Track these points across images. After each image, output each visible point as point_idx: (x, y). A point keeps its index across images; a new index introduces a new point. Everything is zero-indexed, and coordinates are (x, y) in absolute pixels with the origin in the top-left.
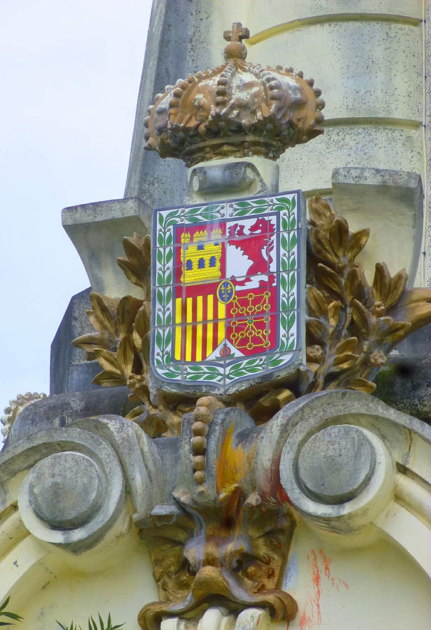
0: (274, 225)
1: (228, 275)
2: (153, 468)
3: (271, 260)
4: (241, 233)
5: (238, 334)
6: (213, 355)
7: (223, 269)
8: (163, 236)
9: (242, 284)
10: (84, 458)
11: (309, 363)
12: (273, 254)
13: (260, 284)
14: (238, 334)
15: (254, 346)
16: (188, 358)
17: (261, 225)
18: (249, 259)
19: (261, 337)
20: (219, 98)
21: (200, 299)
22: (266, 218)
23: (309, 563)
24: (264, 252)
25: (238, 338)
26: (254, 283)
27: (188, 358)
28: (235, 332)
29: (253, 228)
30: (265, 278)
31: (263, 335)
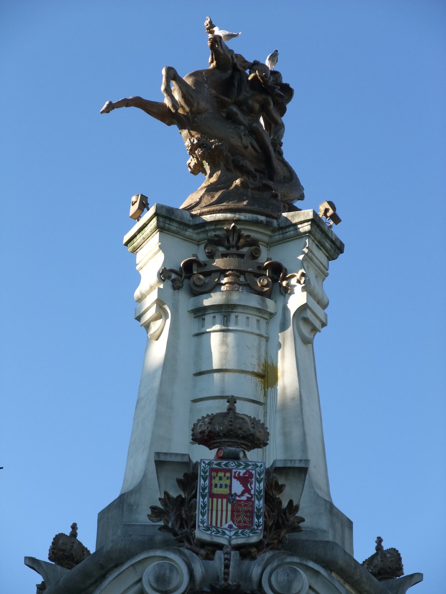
0: (253, 474)
1: (233, 492)
2: (253, 565)
3: (252, 489)
4: (239, 474)
5: (237, 519)
6: (226, 526)
7: (230, 490)
8: (204, 470)
9: (239, 496)
10: (163, 562)
11: (176, 291)
12: (253, 486)
13: (240, 482)
14: (237, 519)
15: (244, 524)
16: (214, 524)
17: (248, 473)
18: (240, 484)
19: (247, 521)
20: (230, 423)
21: (220, 500)
22: (250, 471)
23: (295, 391)
24: (249, 485)
25: (237, 520)
26: (244, 498)
27: (214, 524)
28: (236, 517)
29: (245, 474)
30: (249, 496)
31: (241, 510)
